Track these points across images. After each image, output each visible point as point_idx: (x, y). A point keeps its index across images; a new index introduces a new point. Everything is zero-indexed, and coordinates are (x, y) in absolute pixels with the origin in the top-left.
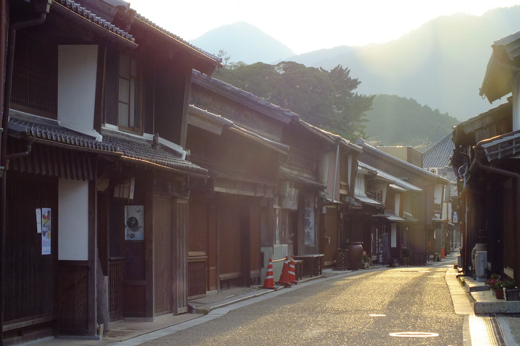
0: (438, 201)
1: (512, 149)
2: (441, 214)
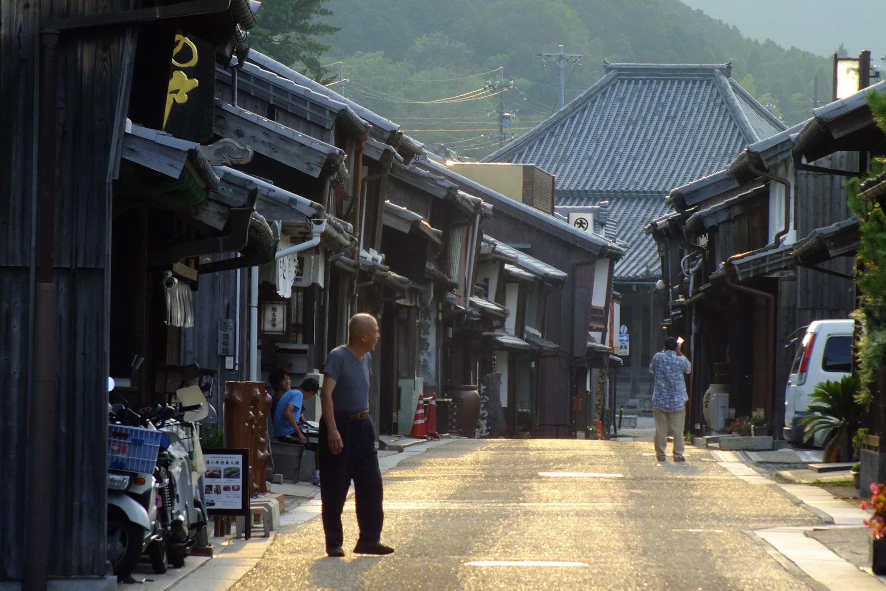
0: (598, 300)
1: (765, 267)
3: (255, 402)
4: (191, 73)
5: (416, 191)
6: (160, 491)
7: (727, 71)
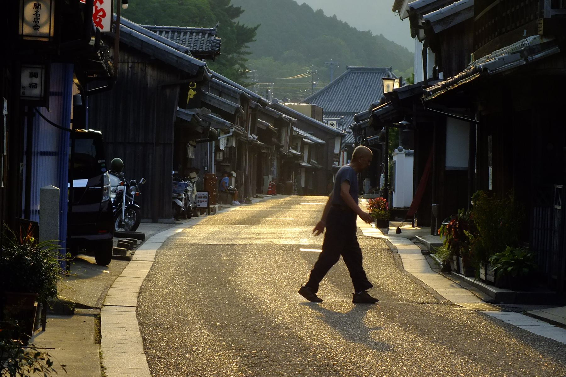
0: (337, 151)
2: (339, 162)
3: (212, 179)
4: (194, 90)
5: (268, 116)
6: (185, 199)
7: (390, 69)
